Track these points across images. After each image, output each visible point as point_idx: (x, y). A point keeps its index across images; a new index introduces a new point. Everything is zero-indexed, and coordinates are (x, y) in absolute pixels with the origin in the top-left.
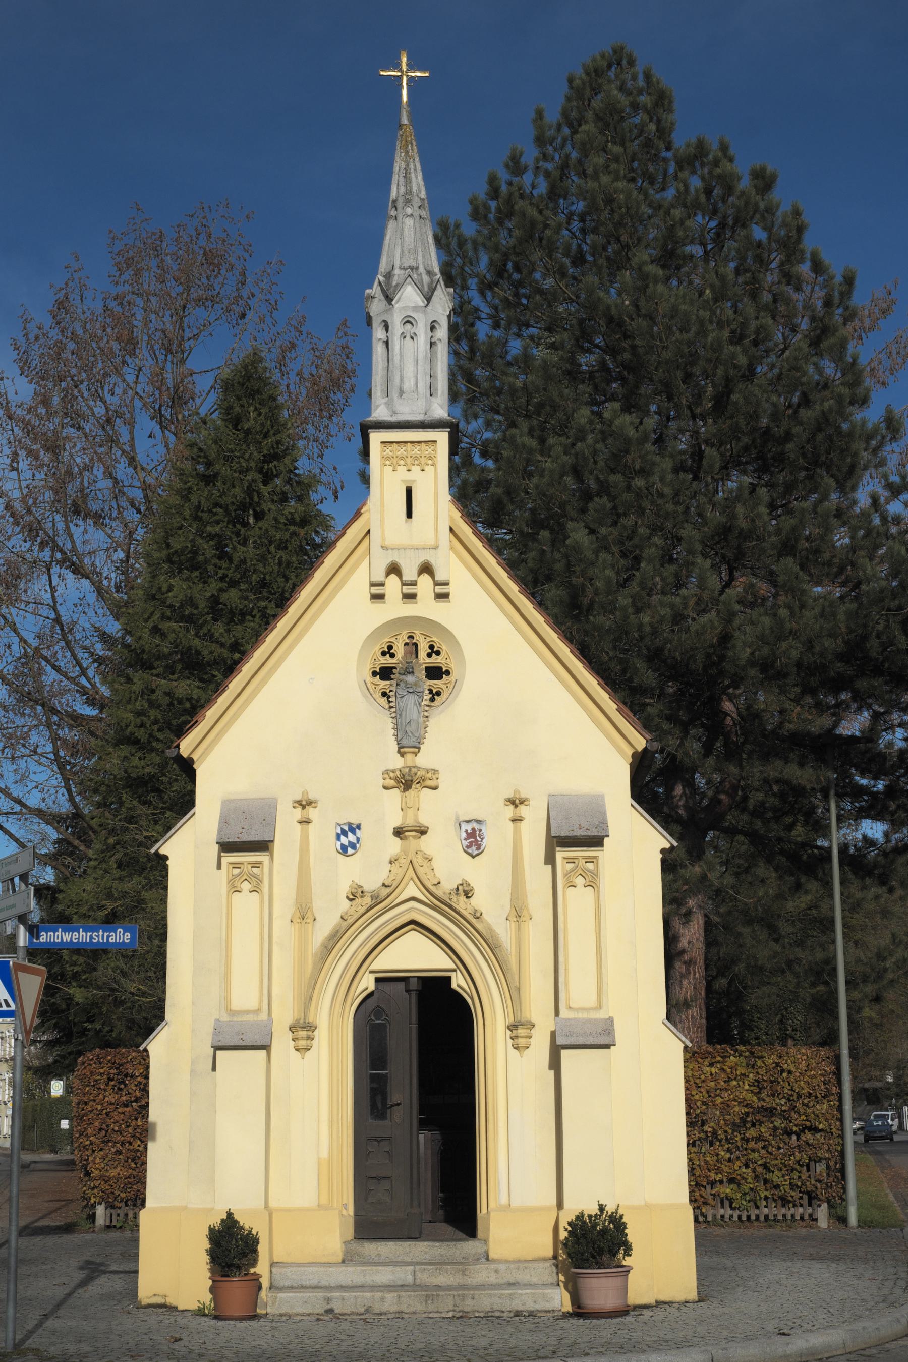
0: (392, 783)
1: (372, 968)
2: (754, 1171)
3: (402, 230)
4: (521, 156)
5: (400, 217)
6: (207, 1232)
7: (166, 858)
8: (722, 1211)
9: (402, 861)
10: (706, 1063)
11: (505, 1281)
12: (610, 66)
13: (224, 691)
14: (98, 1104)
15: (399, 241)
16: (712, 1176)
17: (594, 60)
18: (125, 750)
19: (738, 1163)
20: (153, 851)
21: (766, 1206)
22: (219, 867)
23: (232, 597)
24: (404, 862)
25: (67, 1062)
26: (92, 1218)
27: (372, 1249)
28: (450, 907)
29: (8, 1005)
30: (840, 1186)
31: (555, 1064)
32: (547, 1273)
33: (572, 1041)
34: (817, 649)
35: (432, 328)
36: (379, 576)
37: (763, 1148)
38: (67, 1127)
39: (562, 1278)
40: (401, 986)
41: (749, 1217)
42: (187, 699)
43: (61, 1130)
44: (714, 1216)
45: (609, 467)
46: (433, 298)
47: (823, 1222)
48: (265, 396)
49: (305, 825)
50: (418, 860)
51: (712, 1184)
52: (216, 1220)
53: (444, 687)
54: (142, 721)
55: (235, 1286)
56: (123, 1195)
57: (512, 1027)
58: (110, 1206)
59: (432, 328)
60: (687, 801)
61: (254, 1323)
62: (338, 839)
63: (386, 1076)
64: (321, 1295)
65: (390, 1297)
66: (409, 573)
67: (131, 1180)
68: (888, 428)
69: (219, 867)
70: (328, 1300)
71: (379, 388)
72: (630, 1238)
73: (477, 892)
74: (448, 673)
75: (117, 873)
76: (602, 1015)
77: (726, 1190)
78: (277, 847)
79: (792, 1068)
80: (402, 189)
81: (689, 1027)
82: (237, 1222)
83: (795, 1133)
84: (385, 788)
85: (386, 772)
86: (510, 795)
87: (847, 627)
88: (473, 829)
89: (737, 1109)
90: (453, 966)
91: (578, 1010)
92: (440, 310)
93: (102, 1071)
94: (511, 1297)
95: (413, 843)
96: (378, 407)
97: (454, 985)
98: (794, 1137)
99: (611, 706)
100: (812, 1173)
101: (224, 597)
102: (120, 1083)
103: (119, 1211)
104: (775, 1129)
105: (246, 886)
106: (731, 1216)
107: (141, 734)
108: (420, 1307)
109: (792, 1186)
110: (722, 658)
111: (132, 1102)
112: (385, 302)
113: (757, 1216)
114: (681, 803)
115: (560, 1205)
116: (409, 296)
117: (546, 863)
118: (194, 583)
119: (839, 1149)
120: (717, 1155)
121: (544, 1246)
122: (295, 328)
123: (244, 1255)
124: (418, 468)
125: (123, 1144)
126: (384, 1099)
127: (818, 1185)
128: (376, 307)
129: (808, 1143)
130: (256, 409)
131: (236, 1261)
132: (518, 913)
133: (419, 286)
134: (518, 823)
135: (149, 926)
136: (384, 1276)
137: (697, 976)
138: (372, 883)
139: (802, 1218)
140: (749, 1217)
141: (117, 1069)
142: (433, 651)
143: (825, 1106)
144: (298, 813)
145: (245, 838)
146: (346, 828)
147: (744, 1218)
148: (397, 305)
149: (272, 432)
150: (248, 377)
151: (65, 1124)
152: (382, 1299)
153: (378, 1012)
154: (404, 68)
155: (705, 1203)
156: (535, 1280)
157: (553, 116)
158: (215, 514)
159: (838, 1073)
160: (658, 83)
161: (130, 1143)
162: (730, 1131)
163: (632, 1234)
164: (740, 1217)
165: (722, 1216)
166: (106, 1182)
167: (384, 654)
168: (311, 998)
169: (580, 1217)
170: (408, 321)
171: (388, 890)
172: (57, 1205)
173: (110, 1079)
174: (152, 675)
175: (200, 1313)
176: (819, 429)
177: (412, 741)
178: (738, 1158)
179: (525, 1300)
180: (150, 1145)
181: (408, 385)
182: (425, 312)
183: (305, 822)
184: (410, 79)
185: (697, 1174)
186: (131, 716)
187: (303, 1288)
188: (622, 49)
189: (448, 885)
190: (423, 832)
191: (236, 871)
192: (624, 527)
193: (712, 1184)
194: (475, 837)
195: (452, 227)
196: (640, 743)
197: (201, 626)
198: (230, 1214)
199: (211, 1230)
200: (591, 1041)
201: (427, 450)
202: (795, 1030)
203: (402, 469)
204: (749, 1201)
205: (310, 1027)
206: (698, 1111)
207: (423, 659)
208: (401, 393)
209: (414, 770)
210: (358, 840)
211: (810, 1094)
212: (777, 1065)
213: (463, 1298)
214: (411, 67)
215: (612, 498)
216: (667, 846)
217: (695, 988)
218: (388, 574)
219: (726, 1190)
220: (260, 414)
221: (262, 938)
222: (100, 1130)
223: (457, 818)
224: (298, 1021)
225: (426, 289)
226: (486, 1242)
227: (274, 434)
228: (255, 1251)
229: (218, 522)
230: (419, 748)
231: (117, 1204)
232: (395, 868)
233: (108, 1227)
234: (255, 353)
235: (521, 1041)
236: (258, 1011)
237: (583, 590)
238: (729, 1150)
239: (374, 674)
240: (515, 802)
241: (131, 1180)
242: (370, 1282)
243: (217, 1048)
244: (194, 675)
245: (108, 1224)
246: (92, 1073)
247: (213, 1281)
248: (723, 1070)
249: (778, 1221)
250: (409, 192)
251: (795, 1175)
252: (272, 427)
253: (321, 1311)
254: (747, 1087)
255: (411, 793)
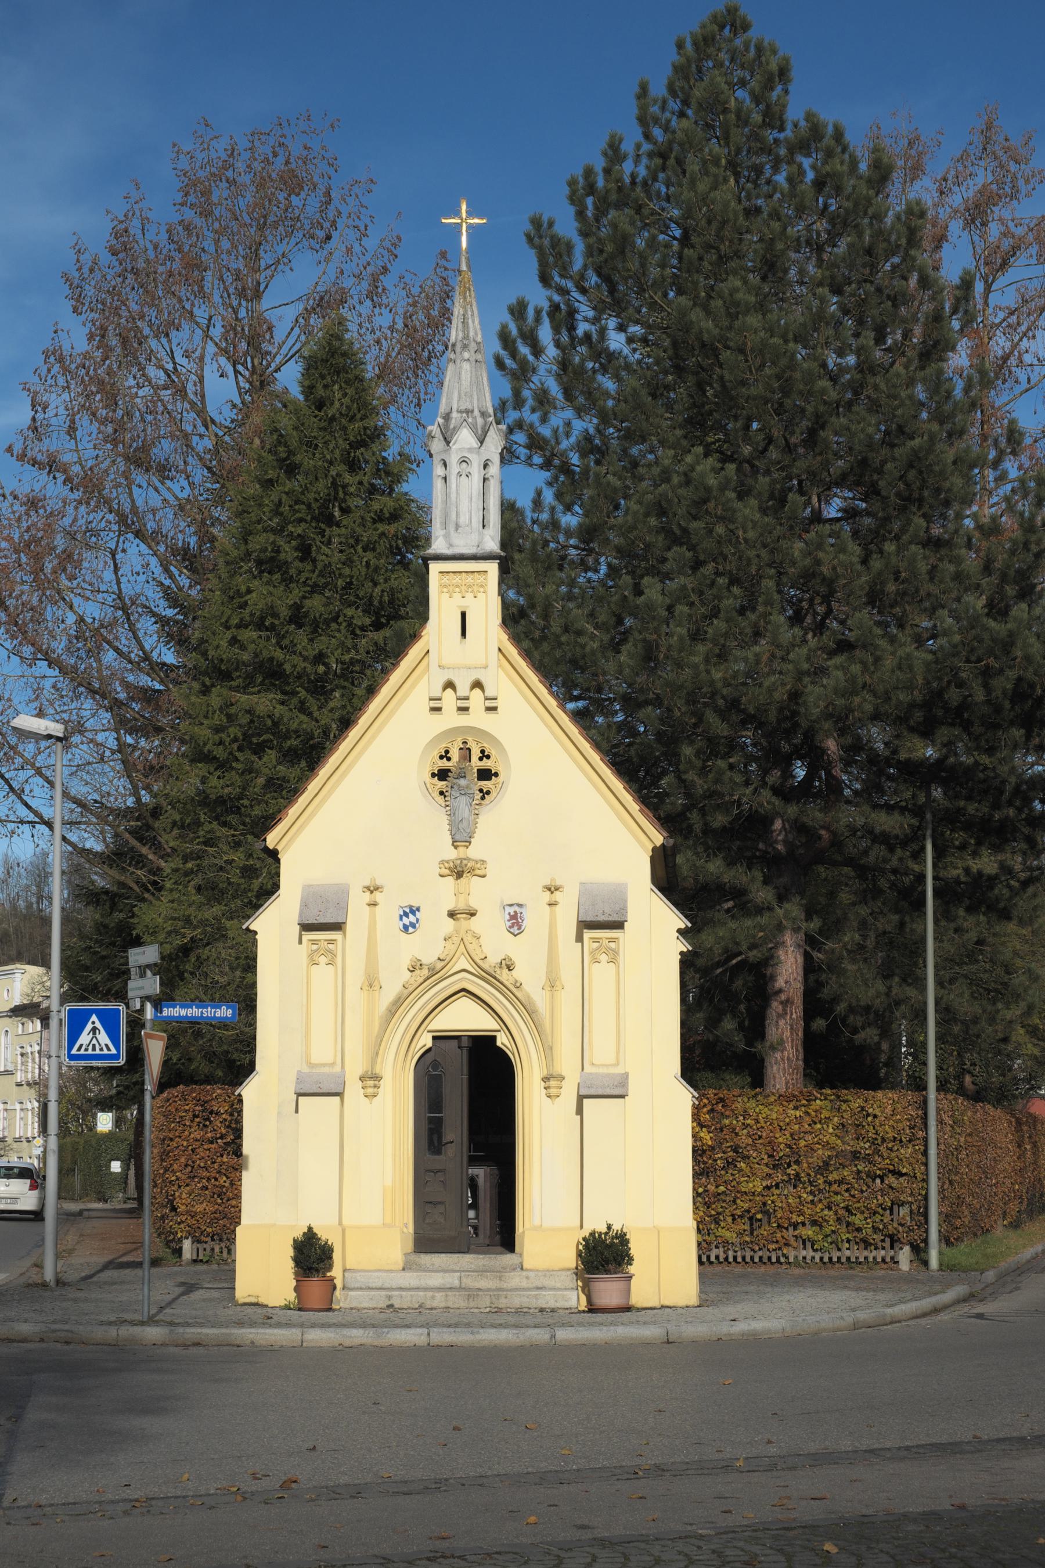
0: (447, 872)
1: (429, 1028)
2: (836, 1213)
3: (460, 374)
4: (620, 142)
5: (458, 361)
6: (292, 1242)
7: (256, 933)
8: (804, 1253)
9: (455, 938)
10: (791, 1106)
11: (534, 1285)
12: (722, 27)
13: (303, 792)
14: (183, 1140)
15: (457, 385)
16: (795, 1218)
17: (703, 26)
18: (202, 769)
19: (820, 1206)
20: (244, 927)
21: (848, 1249)
22: (300, 942)
23: (315, 605)
24: (456, 940)
25: (132, 1093)
26: (179, 1252)
27: (427, 1259)
28: (495, 978)
29: (109, 1049)
30: (923, 1230)
31: (580, 1111)
32: (569, 1280)
33: (592, 1092)
34: (894, 701)
35: (485, 466)
36: (437, 693)
37: (847, 1190)
38: (119, 1170)
39: (580, 1284)
40: (455, 1043)
41: (830, 1259)
42: (269, 716)
43: (112, 1174)
44: (796, 1257)
45: (690, 514)
46: (487, 439)
47: (905, 1265)
48: (351, 376)
49: (372, 908)
50: (468, 938)
51: (795, 1226)
52: (299, 1233)
53: (493, 787)
54: (221, 738)
55: (314, 1284)
56: (209, 1230)
57: (546, 1079)
58: (197, 1241)
59: (485, 466)
60: (786, 836)
61: (330, 1314)
62: (401, 919)
63: (441, 1118)
64: (384, 1293)
65: (439, 1296)
66: (463, 689)
67: (217, 1215)
68: (1009, 440)
69: (300, 942)
70: (389, 1297)
71: (438, 521)
72: (632, 1252)
73: (517, 964)
74: (496, 775)
75: (196, 898)
76: (619, 1070)
77: (808, 1232)
78: (349, 927)
79: (877, 1112)
80: (461, 335)
81: (784, 1069)
82: (316, 1234)
83: (879, 1176)
84: (441, 876)
85: (442, 862)
86: (547, 882)
87: (924, 679)
88: (515, 912)
89: (820, 1152)
90: (498, 1028)
91: (598, 1066)
92: (493, 449)
93: (187, 1108)
94: (536, 1297)
95: (464, 923)
96: (437, 538)
97: (499, 1044)
98: (878, 1181)
99: (635, 807)
100: (895, 1217)
101: (308, 603)
102: (206, 1120)
103: (205, 1246)
104: (859, 1172)
105: (323, 960)
106: (813, 1258)
107: (220, 753)
108: (462, 1304)
109: (875, 1229)
110: (795, 713)
111: (217, 1139)
112: (444, 443)
113: (839, 1258)
114: (780, 838)
115: (582, 1227)
116: (465, 438)
117: (577, 941)
118: (274, 586)
119: (924, 1193)
120: (800, 1197)
121: (569, 1258)
122: (389, 251)
123: (321, 1260)
124: (472, 595)
125: (209, 1179)
126: (440, 1138)
127: (900, 1229)
128: (437, 445)
129: (891, 1187)
130: (341, 388)
131: (315, 1265)
132: (552, 984)
133: (473, 428)
134: (554, 908)
135: (230, 955)
136: (436, 1280)
137: (794, 1016)
138: (429, 958)
139: (883, 1260)
140: (830, 1259)
141: (202, 1106)
142: (484, 755)
143: (909, 1150)
144: (367, 897)
145: (322, 920)
146: (408, 910)
147: (826, 1260)
148: (454, 447)
149: (358, 416)
150: (333, 353)
151: (116, 1166)
152: (433, 1297)
153: (435, 1065)
154: (464, 215)
155: (787, 1245)
156: (558, 1285)
157: (658, 89)
158: (299, 511)
159: (925, 1118)
160: (768, 64)
161: (216, 1179)
162: (813, 1174)
163: (635, 1249)
164: (821, 1259)
165: (804, 1258)
166: (192, 1217)
167: (441, 757)
168: (377, 1053)
169: (592, 1234)
170: (464, 461)
171: (443, 964)
172: (134, 1246)
173: (195, 1116)
174: (231, 688)
175: (287, 1307)
176: (911, 466)
177: (464, 836)
178: (820, 1201)
179: (548, 1300)
180: (244, 1173)
181: (463, 519)
182: (478, 453)
183: (373, 904)
184: (470, 227)
185: (779, 1216)
186: (208, 732)
187: (370, 1289)
188: (736, 10)
189: (494, 959)
190: (473, 915)
191: (315, 947)
192: (704, 576)
193: (795, 1226)
194: (516, 919)
195: (545, 225)
196: (659, 839)
197: (284, 637)
198: (310, 1229)
199: (295, 1241)
200: (608, 1092)
201: (479, 579)
202: (974, 1064)
203: (457, 596)
204: (831, 1243)
205: (377, 1078)
206: (781, 1154)
207: (476, 763)
208: (457, 526)
209: (465, 862)
210: (418, 920)
211: (895, 1138)
212: (863, 1109)
213: (498, 1297)
214: (470, 214)
215: (692, 548)
216: (683, 926)
217: (791, 1029)
218: (444, 689)
219: (808, 1232)
220: (345, 395)
221: (336, 1004)
222: (186, 1166)
223: (502, 902)
224: (367, 1072)
225: (480, 432)
226: (521, 1255)
227: (362, 419)
228: (331, 1258)
229: (301, 520)
230: (470, 843)
231: (203, 1238)
232: (449, 943)
233: (195, 1261)
234: (340, 323)
235: (553, 1091)
236: (333, 1064)
237: (657, 648)
238: (811, 1193)
239: (433, 775)
240: (551, 889)
241: (217, 1215)
242: (424, 1285)
243: (299, 1095)
244: (275, 685)
245: (195, 1258)
246: (177, 1109)
247: (297, 1281)
248: (807, 1113)
249: (860, 1263)
250: (466, 337)
251: (878, 1218)
252: (359, 411)
253: (384, 1306)
254: (831, 1130)
255: (463, 880)
